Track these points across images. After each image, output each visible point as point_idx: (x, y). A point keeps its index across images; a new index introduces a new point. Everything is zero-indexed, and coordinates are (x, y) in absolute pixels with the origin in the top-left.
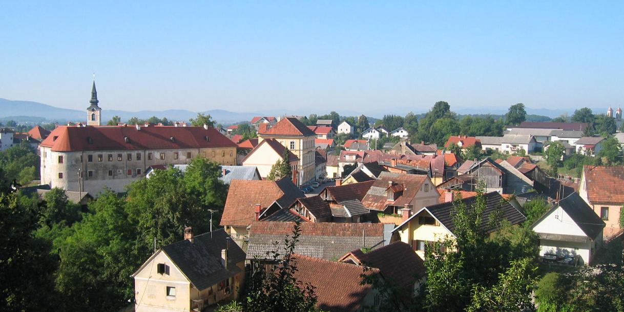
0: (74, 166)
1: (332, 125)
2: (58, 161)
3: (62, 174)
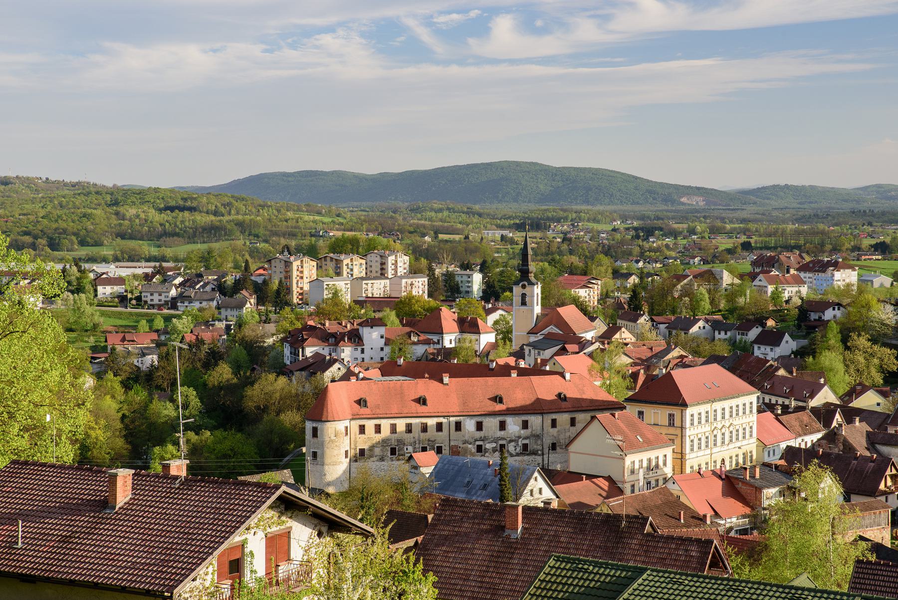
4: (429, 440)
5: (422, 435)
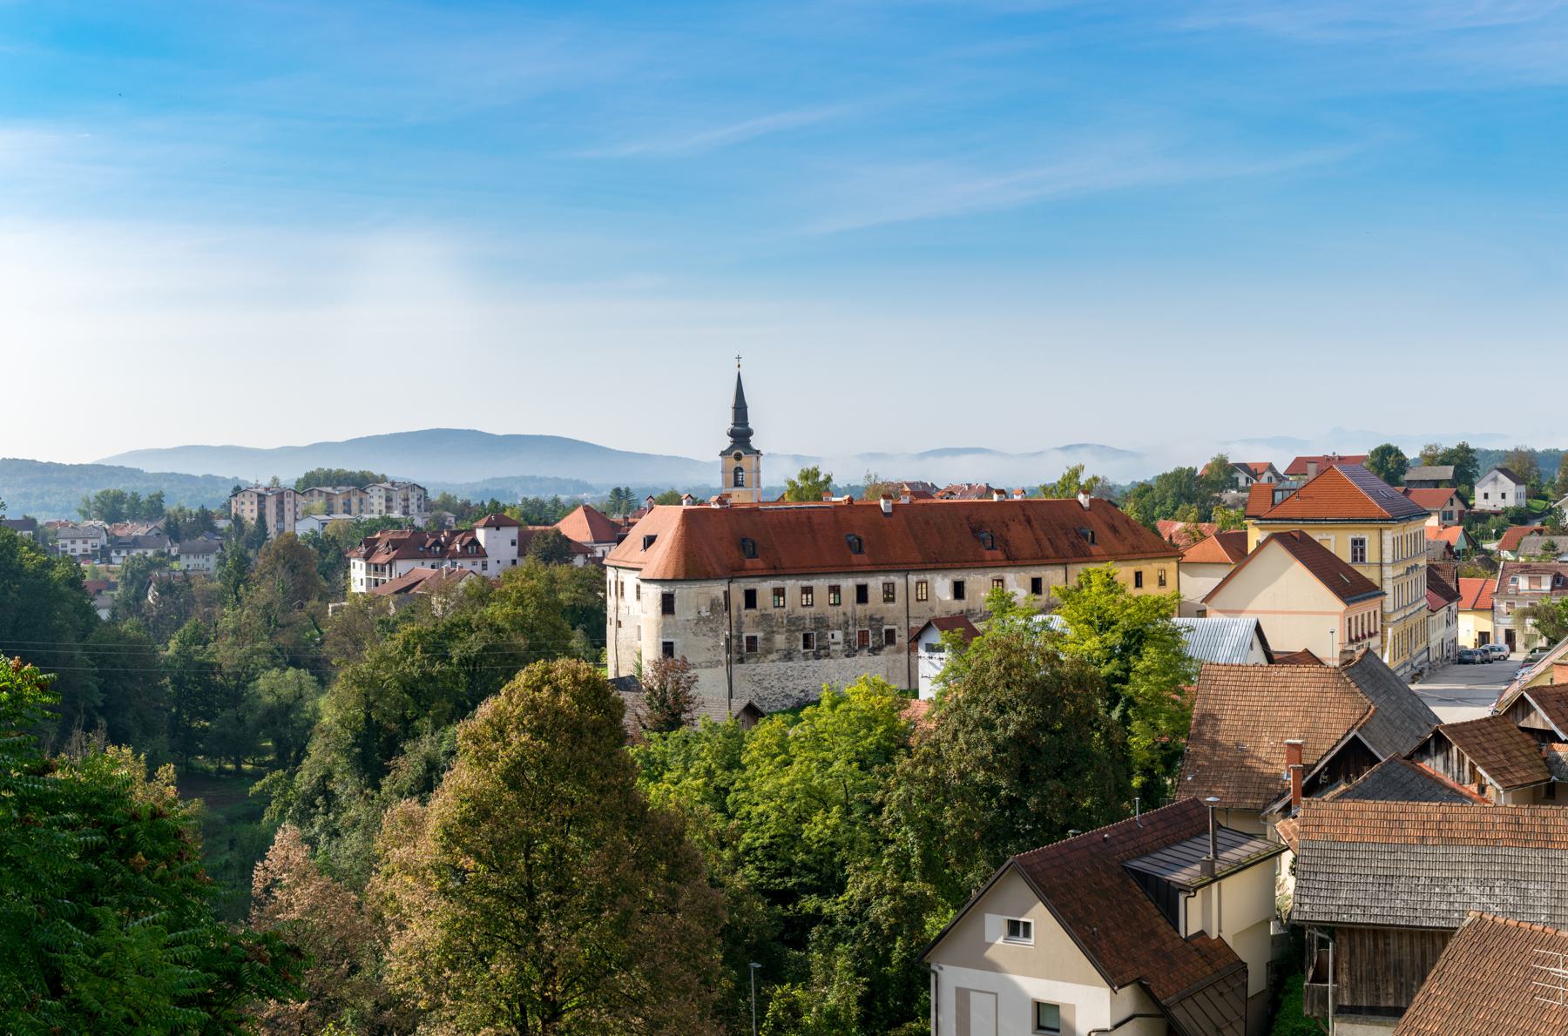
0: (706, 620)
1: (1452, 483)
2: (660, 609)
3: (672, 643)
4: (871, 618)
5: (859, 607)
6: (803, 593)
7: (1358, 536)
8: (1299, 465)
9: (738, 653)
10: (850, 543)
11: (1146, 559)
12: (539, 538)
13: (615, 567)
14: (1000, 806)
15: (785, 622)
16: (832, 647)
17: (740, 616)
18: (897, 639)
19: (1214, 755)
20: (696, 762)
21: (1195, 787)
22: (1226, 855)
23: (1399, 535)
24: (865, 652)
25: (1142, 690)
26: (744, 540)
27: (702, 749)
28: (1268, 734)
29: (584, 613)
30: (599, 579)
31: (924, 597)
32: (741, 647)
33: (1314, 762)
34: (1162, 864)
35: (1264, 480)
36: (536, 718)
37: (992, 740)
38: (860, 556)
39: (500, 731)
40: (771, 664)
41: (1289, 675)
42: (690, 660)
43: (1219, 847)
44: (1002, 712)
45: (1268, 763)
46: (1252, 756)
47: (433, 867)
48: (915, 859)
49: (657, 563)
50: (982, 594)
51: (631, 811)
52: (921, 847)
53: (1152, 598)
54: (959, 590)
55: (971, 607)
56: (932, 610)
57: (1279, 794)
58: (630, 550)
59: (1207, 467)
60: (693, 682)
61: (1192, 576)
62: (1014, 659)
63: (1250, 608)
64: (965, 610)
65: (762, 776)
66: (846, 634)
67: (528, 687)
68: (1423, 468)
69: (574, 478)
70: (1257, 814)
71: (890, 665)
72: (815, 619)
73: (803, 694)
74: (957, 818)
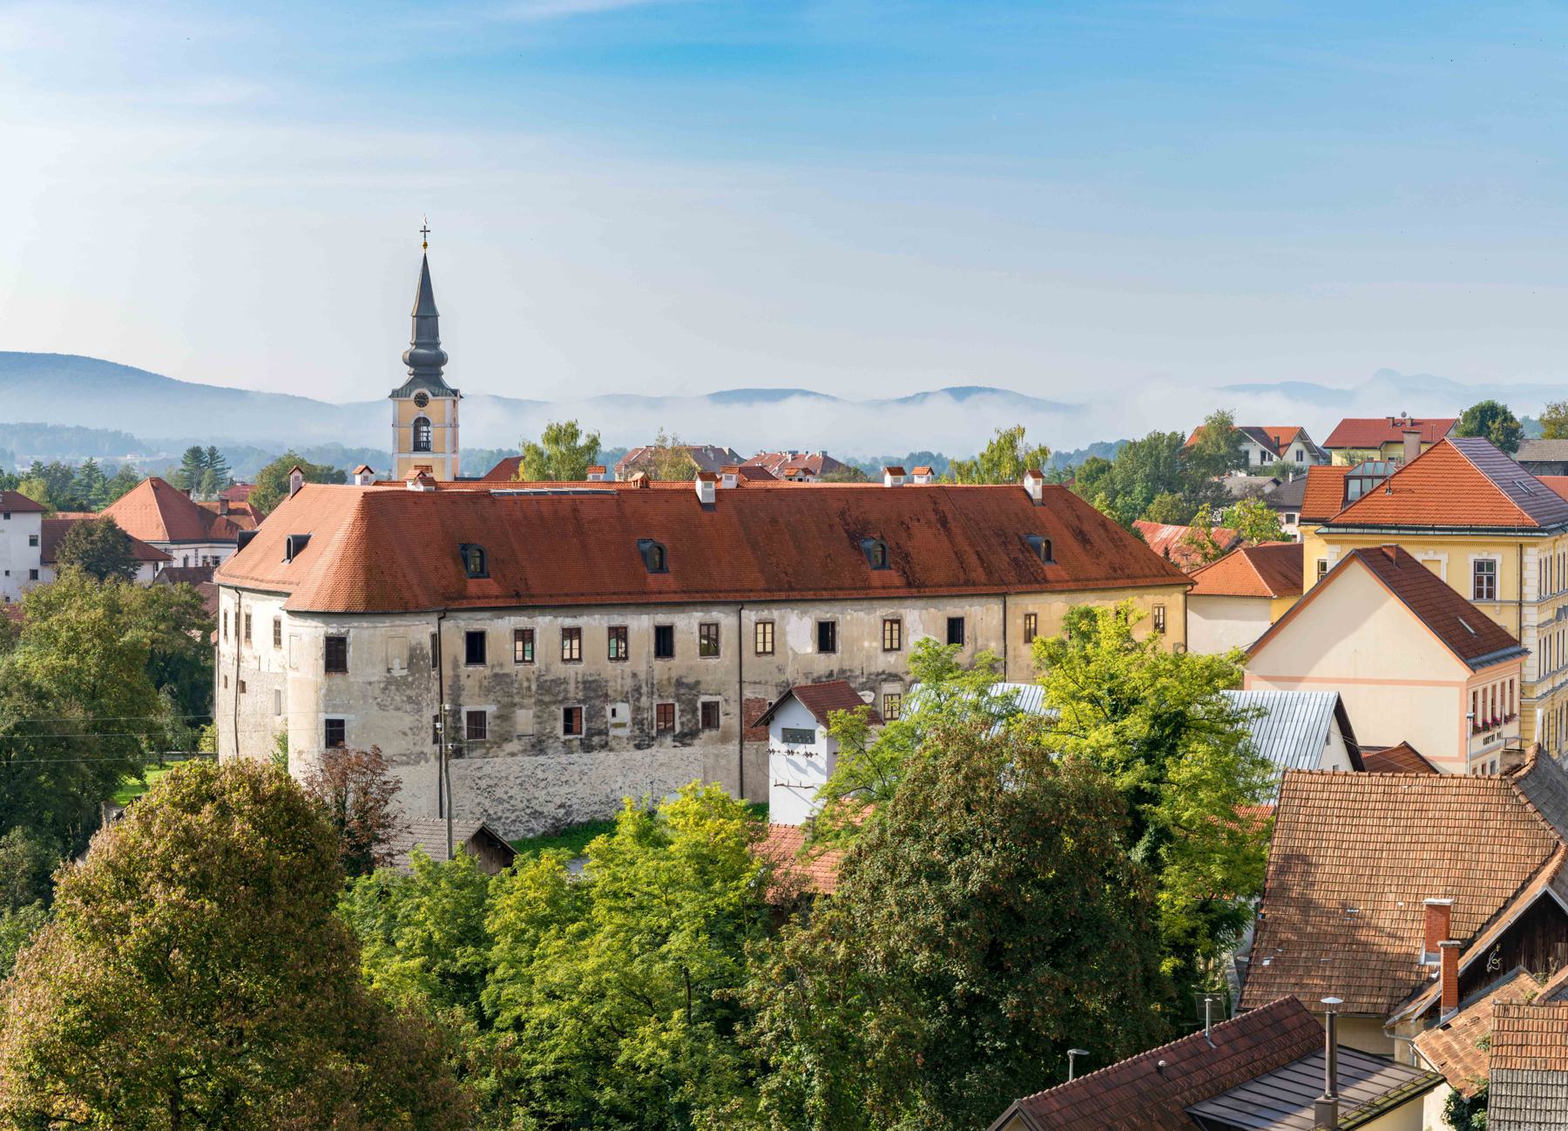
0: (400, 684)
2: (322, 663)
3: (341, 723)
4: (679, 683)
5: (659, 665)
6: (564, 638)
7: (1484, 555)
8: (1351, 434)
9: (454, 740)
10: (644, 554)
11: (1133, 588)
12: (78, 534)
13: (236, 589)
14: (952, 1009)
15: (534, 687)
16: (613, 732)
17: (457, 677)
18: (723, 720)
19: (1307, 923)
20: (406, 930)
21: (1275, 977)
22: (1349, 1092)
23: (1547, 555)
24: (668, 740)
25: (1186, 815)
26: (465, 547)
27: (418, 907)
28: (1394, 888)
29: (167, 665)
30: (193, 607)
31: (769, 648)
32: (458, 729)
33: (1470, 935)
34: (1251, 1109)
35: (1290, 457)
36: (194, 860)
37: (942, 898)
38: (661, 577)
39: (129, 884)
40: (509, 760)
41: (1428, 790)
42: (387, 752)
43: (1339, 1079)
44: (958, 852)
45: (1394, 937)
46: (1369, 926)
47: (13, 1114)
48: (814, 1101)
49: (317, 584)
50: (866, 644)
51: (353, 1021)
52: (826, 1079)
53: (1201, 661)
54: (826, 637)
55: (846, 667)
56: (780, 670)
57: (1414, 989)
58: (262, 560)
59: (1198, 431)
60: (393, 790)
61: (1207, 617)
62: (982, 763)
63: (1314, 673)
64: (836, 671)
65: (543, 957)
66: (637, 710)
67: (175, 805)
68: (1546, 442)
69: (111, 429)
70: (1377, 1021)
71: (710, 762)
72: (584, 682)
73: (562, 811)
74: (886, 1032)
